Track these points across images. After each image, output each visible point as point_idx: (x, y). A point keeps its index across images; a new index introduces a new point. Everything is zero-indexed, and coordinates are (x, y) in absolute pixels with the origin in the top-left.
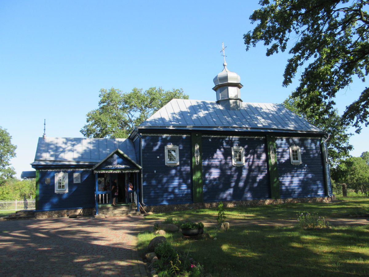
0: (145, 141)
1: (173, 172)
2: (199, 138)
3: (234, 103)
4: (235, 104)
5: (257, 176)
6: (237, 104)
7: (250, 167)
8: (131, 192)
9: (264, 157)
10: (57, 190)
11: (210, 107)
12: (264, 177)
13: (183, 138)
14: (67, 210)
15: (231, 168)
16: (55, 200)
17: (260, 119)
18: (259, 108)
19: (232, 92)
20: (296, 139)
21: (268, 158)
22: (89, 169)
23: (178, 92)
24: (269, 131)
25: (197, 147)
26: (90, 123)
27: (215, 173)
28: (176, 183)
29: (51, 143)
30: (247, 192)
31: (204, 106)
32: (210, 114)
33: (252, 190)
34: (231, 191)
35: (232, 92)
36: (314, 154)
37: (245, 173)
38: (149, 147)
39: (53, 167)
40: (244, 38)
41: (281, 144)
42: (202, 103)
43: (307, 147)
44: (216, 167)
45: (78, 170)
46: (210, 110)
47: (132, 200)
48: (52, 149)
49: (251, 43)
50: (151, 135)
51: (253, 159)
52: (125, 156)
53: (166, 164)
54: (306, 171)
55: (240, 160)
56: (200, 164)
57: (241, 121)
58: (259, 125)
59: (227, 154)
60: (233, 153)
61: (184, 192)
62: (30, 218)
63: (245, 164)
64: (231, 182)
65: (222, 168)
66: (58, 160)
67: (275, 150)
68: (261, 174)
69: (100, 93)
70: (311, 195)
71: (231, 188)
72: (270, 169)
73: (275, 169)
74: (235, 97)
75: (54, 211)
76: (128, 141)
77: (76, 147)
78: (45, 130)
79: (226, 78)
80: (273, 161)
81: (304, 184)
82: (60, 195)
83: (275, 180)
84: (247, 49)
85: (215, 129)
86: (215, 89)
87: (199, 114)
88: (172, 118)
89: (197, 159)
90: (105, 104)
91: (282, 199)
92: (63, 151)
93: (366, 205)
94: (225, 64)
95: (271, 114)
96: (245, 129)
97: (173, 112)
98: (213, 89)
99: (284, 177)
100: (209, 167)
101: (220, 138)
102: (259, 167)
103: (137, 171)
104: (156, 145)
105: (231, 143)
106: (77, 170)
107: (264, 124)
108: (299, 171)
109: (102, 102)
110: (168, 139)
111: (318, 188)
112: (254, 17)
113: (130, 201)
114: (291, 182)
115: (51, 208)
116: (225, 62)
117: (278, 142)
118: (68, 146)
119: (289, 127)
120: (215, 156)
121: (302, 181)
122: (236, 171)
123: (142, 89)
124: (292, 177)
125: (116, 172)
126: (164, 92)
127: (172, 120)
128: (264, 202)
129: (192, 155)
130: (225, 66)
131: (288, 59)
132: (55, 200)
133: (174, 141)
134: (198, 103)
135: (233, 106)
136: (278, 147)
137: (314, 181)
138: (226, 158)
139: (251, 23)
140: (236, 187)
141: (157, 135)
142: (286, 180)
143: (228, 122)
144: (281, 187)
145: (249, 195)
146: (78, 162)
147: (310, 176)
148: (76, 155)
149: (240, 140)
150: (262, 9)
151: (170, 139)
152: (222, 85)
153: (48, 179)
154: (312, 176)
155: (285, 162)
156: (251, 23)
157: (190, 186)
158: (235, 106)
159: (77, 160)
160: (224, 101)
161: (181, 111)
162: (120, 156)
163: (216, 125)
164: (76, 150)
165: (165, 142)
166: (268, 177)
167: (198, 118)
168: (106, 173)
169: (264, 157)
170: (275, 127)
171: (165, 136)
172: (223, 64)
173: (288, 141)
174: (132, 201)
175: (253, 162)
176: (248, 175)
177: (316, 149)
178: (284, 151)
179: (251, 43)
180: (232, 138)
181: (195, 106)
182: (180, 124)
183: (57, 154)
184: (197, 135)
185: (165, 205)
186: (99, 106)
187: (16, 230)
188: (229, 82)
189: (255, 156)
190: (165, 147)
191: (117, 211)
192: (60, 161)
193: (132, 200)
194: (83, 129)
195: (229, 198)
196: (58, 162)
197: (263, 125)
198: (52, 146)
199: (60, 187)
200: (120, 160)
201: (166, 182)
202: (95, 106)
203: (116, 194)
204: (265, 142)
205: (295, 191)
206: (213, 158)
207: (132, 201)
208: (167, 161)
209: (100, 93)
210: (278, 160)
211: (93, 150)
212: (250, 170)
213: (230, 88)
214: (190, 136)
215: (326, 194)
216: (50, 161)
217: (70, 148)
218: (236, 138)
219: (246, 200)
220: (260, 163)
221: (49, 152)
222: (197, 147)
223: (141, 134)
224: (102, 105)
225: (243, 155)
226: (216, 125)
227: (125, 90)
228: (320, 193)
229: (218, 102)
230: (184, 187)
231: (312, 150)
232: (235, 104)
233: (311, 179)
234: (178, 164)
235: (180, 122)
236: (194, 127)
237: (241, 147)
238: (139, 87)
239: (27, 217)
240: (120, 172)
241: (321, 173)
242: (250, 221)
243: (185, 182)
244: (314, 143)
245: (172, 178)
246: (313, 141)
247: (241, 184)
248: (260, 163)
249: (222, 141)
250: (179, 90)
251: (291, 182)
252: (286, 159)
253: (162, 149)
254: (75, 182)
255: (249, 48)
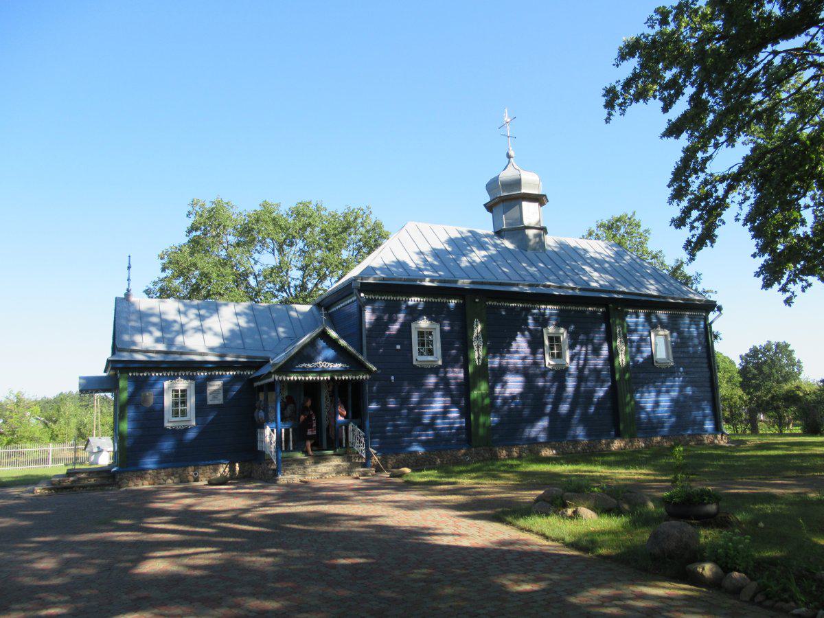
0: (373, 311)
1: (432, 380)
2: (479, 307)
3: (536, 236)
4: (537, 239)
5: (594, 391)
6: (540, 239)
7: (580, 370)
8: (341, 424)
9: (605, 351)
10: (169, 422)
11: (487, 243)
12: (607, 393)
13: (448, 307)
14: (195, 466)
15: (544, 374)
16: (167, 445)
17: (591, 272)
18: (579, 249)
19: (530, 213)
20: (663, 315)
21: (613, 354)
22: (242, 373)
23: (362, 212)
24: (616, 296)
25: (478, 328)
26: (169, 273)
27: (514, 385)
28: (438, 404)
29: (150, 312)
30: (578, 425)
31: (476, 240)
32: (491, 257)
33: (586, 420)
34: (543, 423)
35: (530, 213)
36: (694, 346)
37: (571, 385)
38: (381, 326)
39: (165, 366)
40: (604, 96)
41: (637, 324)
42: (470, 234)
43: (683, 332)
44: (517, 371)
45: (217, 373)
46: (489, 249)
47: (344, 441)
48: (154, 324)
49: (617, 108)
50: (383, 298)
51: (586, 354)
52: (343, 342)
53: (414, 363)
54: (682, 382)
55: (560, 356)
56: (485, 363)
57: (519, 275)
58: (594, 284)
59: (536, 344)
60: (547, 342)
61: (454, 423)
62: (107, 488)
63: (573, 368)
64: (546, 404)
65: (528, 374)
66: (174, 349)
67: (625, 336)
68: (602, 387)
69: (190, 208)
70: (693, 430)
71: (545, 415)
72: (617, 377)
73: (627, 376)
74: (537, 224)
75: (164, 468)
76: (314, 309)
77: (208, 323)
78: (129, 280)
79: (517, 183)
80: (622, 359)
81: (679, 407)
82: (179, 433)
83: (628, 398)
84: (608, 120)
85: (515, 289)
86: (489, 207)
87: (471, 255)
88: (422, 263)
89: (477, 354)
90: (199, 233)
91: (640, 438)
92: (182, 331)
93: (818, 450)
94: (512, 153)
95: (607, 262)
96: (570, 292)
97: (418, 250)
98: (485, 205)
99: (642, 393)
100: (502, 371)
101: (523, 309)
102: (596, 372)
103: (364, 377)
104: (394, 321)
105: (543, 321)
106: (219, 374)
107: (602, 282)
108: (670, 381)
109: (193, 228)
110: (421, 307)
111: (705, 416)
112: (629, 50)
113: (341, 445)
114: (657, 404)
115: (159, 462)
116: (511, 148)
117: (630, 320)
118: (191, 320)
119: (648, 289)
120: (514, 347)
121: (675, 402)
122: (554, 379)
123: (278, 205)
124: (658, 393)
125: (320, 379)
126: (327, 213)
127: (423, 267)
128: (608, 445)
129: (466, 346)
130: (512, 159)
131: (683, 148)
132: (167, 445)
133: (431, 312)
134: (461, 233)
135: (535, 243)
136: (632, 331)
137: (696, 401)
138: (534, 352)
139: (614, 65)
140: (554, 415)
141: (395, 299)
142: (648, 400)
143: (532, 275)
144: (639, 414)
145: (580, 431)
146: (222, 356)
147: (689, 391)
148: (216, 342)
149: (561, 314)
150: (642, 37)
151: (424, 308)
152: (505, 198)
153: (150, 396)
154: (693, 392)
155: (643, 362)
156: (614, 65)
157: (465, 413)
158: (538, 243)
159: (222, 350)
160: (517, 231)
161: (434, 249)
162: (332, 343)
163: (511, 280)
164: (210, 329)
165: (414, 314)
166: (613, 393)
167: (472, 264)
168: (298, 379)
169: (605, 351)
170: (623, 289)
171: (413, 301)
172: (508, 154)
173: (648, 317)
174: (344, 445)
175: (586, 360)
176: (577, 388)
177: (698, 337)
178: (642, 339)
179: (617, 108)
180: (545, 309)
181: (456, 238)
182: (440, 276)
183: (169, 336)
184: (477, 300)
185: (416, 452)
186: (186, 236)
187: (225, 537)
188: (524, 190)
189: (590, 348)
190: (413, 325)
191: (323, 468)
192: (182, 353)
193: (344, 441)
194: (152, 287)
195: (542, 437)
196: (177, 356)
197: (601, 285)
198: (155, 320)
199: (176, 414)
200: (330, 353)
201: (420, 402)
202: (179, 237)
203: (309, 433)
204: (606, 318)
205: (664, 422)
206: (509, 352)
207: (344, 445)
208: (418, 358)
209: (190, 208)
210: (632, 358)
211: (249, 329)
212: (581, 378)
213: (525, 205)
214: (461, 301)
215: (718, 429)
216: (158, 352)
217: (196, 323)
218: (550, 309)
219: (575, 442)
220: (599, 363)
221: (150, 333)
222: (478, 328)
223: (362, 295)
224: (194, 234)
225: (567, 347)
226: (511, 280)
227: (243, 205)
228: (709, 426)
229: (499, 233)
230: (454, 414)
231: (691, 338)
232: (537, 239)
233: (691, 397)
234: (440, 363)
235: (440, 271)
236: (473, 283)
237: (562, 330)
238: (272, 200)
239: (98, 486)
240: (329, 378)
241: (708, 384)
242: (438, 479)
243: (455, 403)
244: (695, 325)
245: (429, 395)
246: (692, 318)
247: (564, 408)
248: (599, 363)
249: (526, 315)
250: (362, 210)
251: (657, 404)
252: (645, 355)
253: (406, 329)
254: (209, 402)
255: (611, 117)
